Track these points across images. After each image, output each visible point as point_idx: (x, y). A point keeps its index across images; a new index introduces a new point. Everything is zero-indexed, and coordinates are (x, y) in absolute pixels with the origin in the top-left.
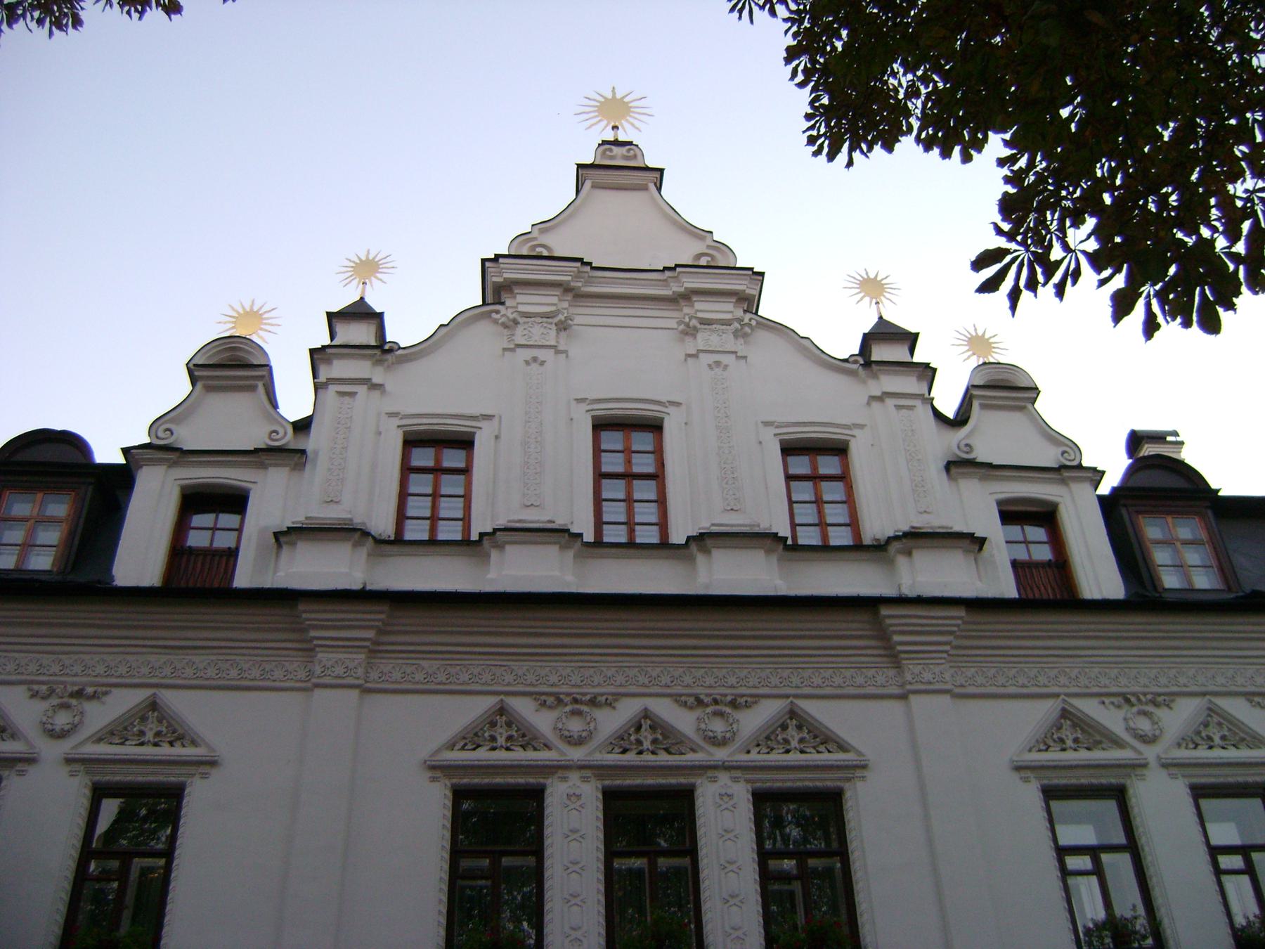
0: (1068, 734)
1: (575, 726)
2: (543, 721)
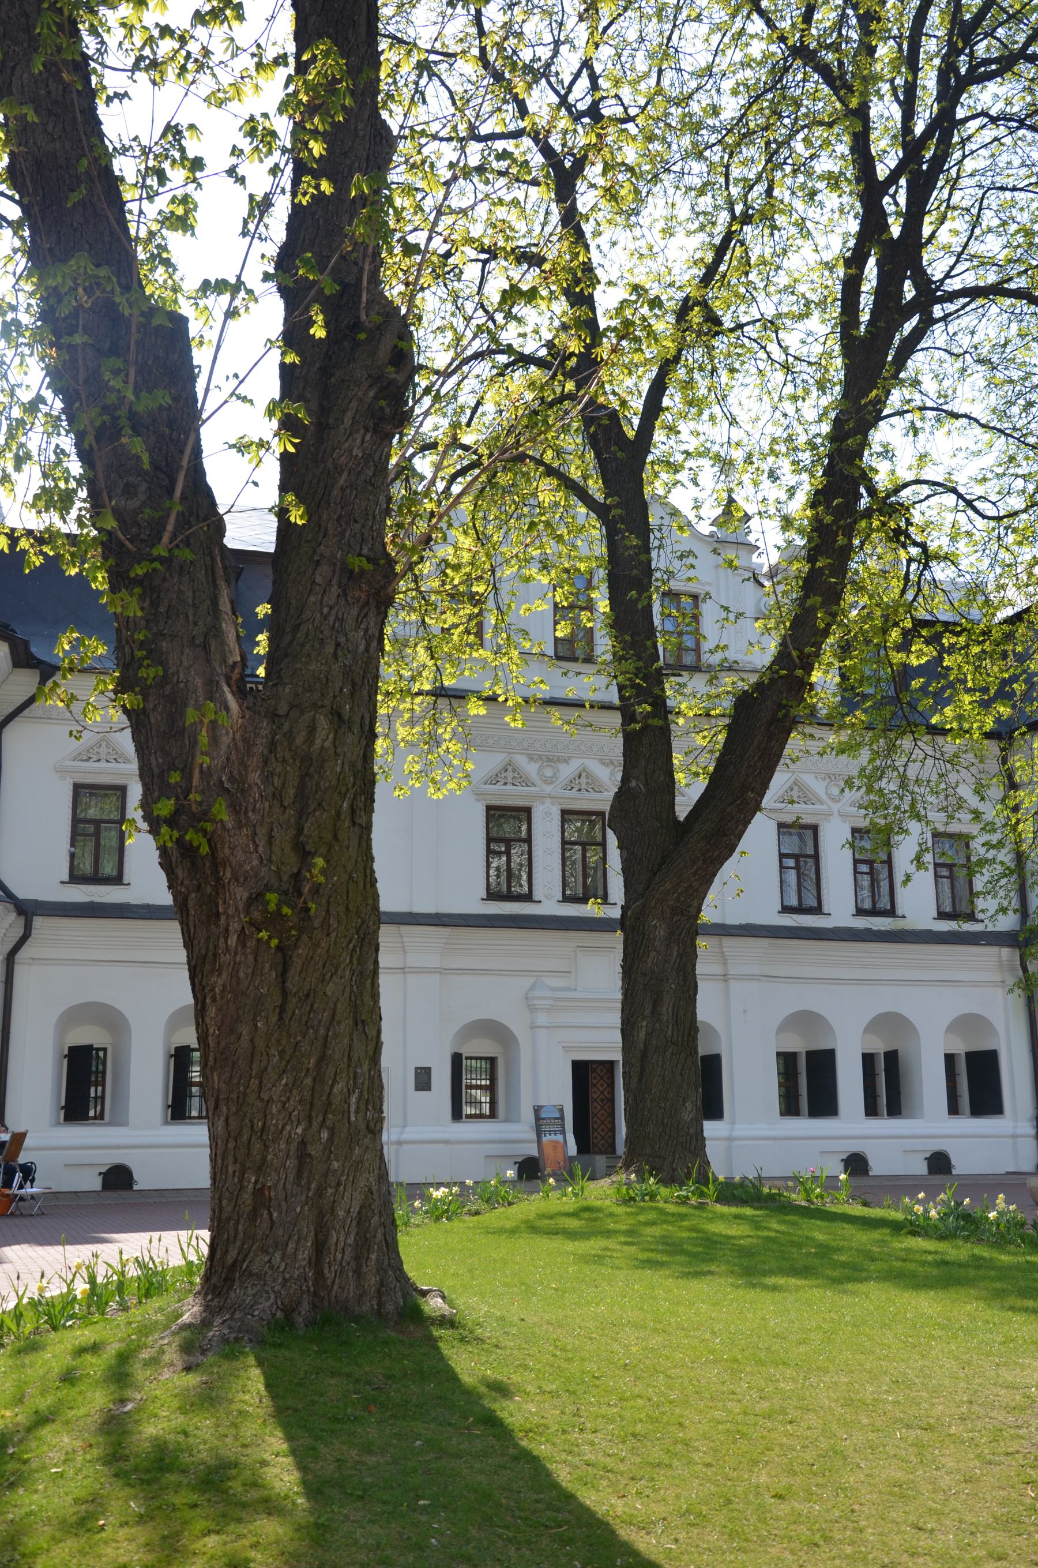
0: (103, 750)
1: (549, 773)
2: (531, 769)
